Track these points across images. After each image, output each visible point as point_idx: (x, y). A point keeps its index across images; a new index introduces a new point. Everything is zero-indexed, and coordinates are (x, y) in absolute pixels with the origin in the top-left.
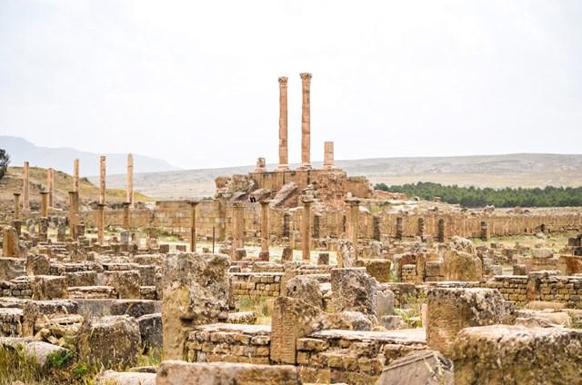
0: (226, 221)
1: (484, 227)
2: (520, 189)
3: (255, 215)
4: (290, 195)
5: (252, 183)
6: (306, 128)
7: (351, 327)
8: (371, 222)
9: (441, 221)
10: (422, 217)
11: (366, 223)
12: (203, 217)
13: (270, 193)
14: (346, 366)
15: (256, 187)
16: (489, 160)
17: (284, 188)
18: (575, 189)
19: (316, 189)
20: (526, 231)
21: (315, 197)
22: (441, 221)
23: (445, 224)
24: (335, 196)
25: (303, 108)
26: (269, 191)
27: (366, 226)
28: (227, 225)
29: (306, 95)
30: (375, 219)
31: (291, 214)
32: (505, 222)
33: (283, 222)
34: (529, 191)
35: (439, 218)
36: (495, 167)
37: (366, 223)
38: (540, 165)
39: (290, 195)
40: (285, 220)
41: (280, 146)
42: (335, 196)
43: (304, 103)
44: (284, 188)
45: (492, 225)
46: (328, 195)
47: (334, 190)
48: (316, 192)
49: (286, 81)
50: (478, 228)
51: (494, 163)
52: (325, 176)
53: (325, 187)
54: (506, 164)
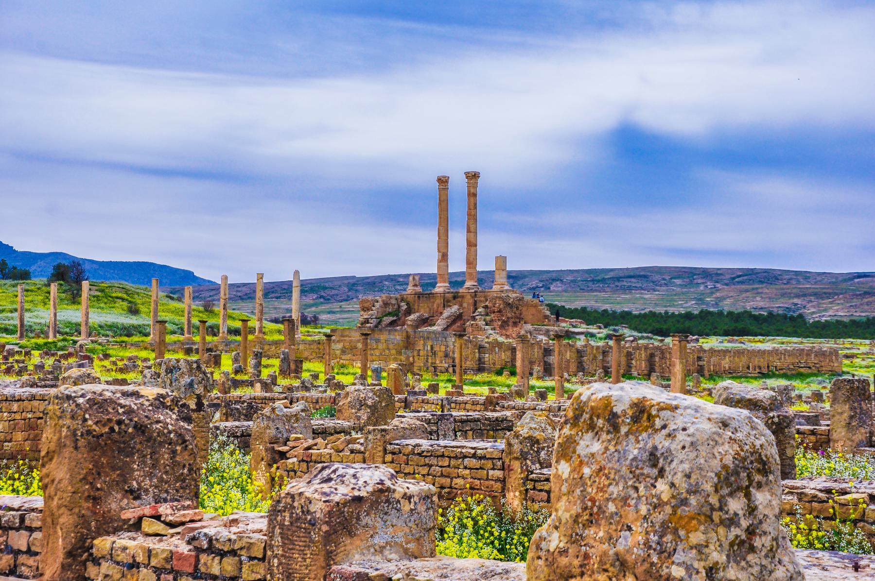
0: (415, 353)
1: (701, 363)
2: (666, 313)
3: (447, 346)
4: (454, 322)
5: (404, 306)
6: (473, 240)
7: (388, 483)
8: (574, 356)
9: (652, 355)
10: (630, 350)
11: (568, 357)
12: (388, 349)
13: (427, 319)
14: (140, 559)
15: (409, 312)
16: (611, 275)
17: (447, 313)
18: (738, 314)
19: (487, 315)
20: (748, 368)
21: (487, 325)
22: (652, 355)
23: (657, 359)
24: (510, 323)
25: (469, 215)
26: (426, 315)
27: (568, 361)
28: (416, 359)
29: (472, 199)
30: (578, 351)
31: (487, 345)
32: (725, 356)
33: (477, 355)
34: (680, 315)
35: (649, 352)
36: (619, 284)
37: (568, 357)
38: (678, 282)
39: (454, 322)
40: (479, 353)
41: (440, 261)
42: (510, 323)
43: (469, 209)
44: (447, 313)
45: (709, 362)
46: (504, 322)
47: (509, 315)
48: (488, 318)
49: (447, 182)
50: (694, 363)
51: (619, 279)
52: (500, 298)
53: (500, 311)
54: (633, 280)
